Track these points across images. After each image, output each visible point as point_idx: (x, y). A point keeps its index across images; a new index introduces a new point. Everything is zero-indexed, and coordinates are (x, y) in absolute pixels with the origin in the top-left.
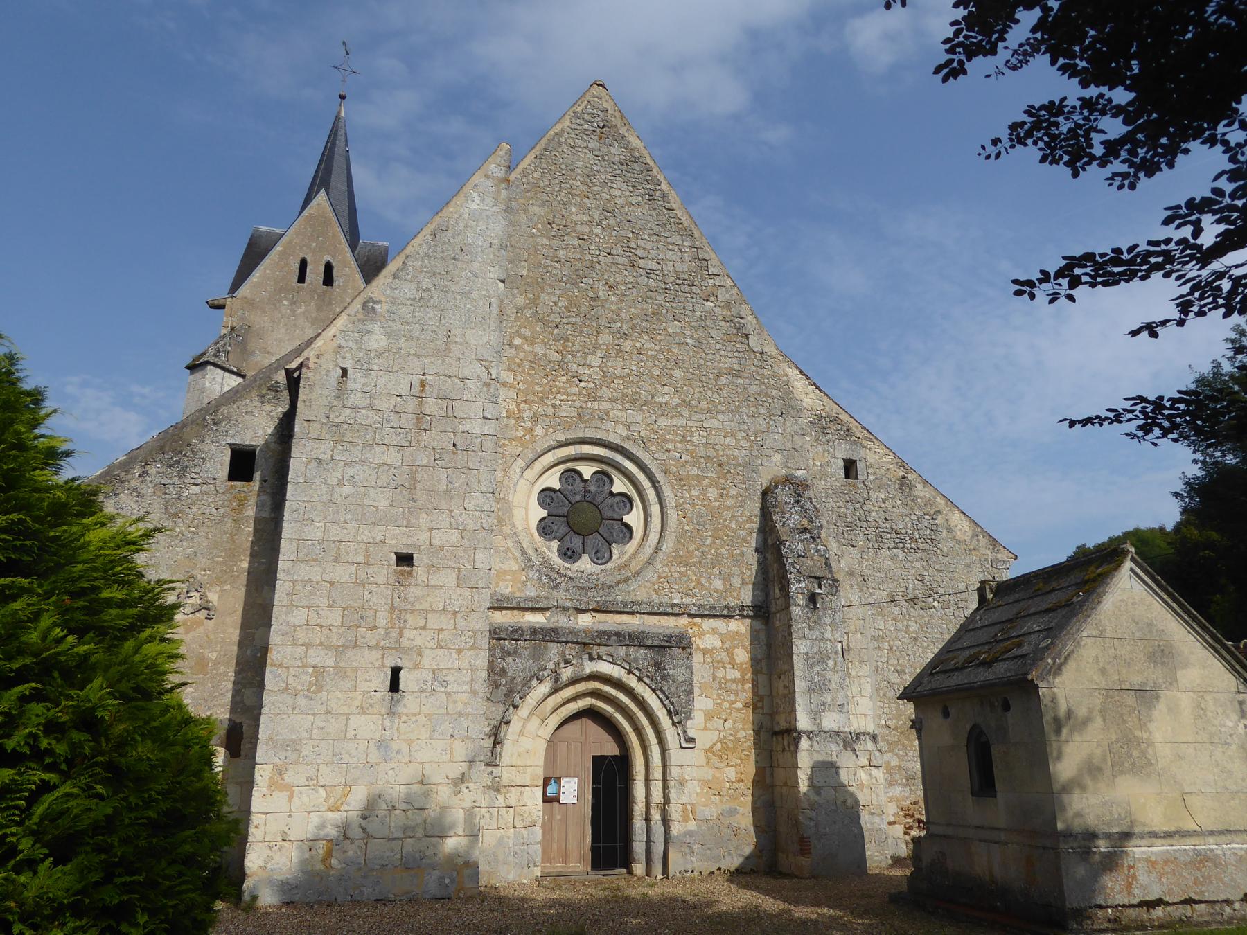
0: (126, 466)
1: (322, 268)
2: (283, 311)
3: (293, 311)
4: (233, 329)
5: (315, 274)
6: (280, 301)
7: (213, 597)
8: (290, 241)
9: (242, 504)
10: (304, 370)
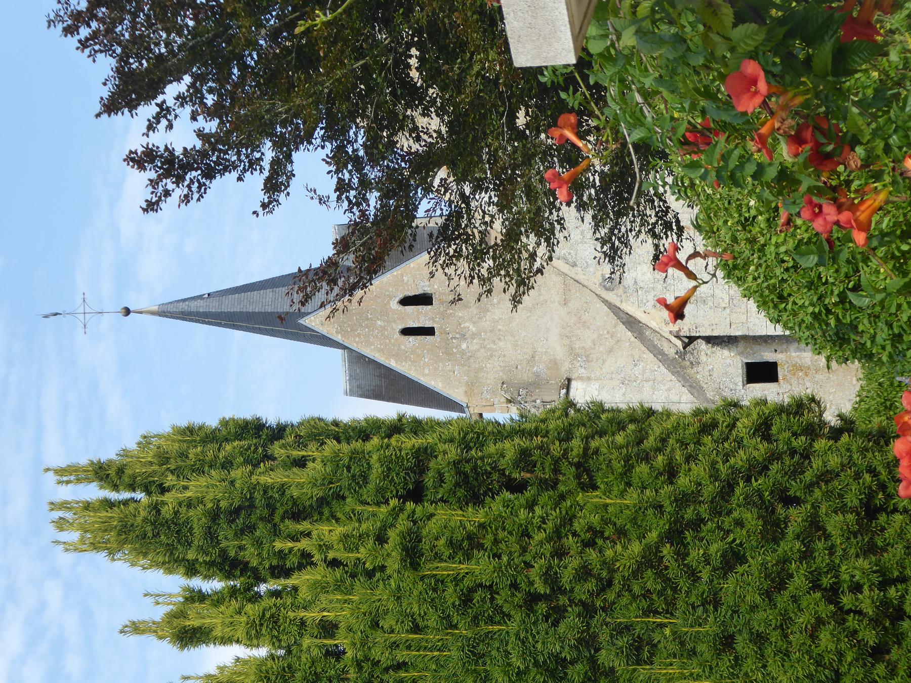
1: (410, 309)
2: (475, 347)
3: (474, 336)
4: (509, 401)
5: (417, 316)
6: (463, 353)
8: (381, 351)
10: (682, 334)
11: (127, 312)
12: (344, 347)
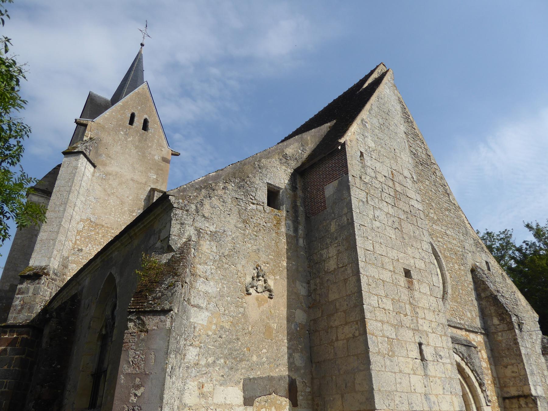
0: (216, 179)
5: (138, 123)
6: (119, 131)
7: (271, 283)
8: (127, 102)
9: (278, 223)
11: (142, 45)
12: (117, 97)
